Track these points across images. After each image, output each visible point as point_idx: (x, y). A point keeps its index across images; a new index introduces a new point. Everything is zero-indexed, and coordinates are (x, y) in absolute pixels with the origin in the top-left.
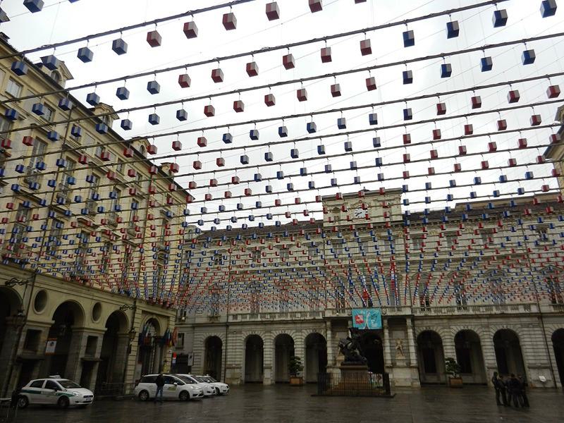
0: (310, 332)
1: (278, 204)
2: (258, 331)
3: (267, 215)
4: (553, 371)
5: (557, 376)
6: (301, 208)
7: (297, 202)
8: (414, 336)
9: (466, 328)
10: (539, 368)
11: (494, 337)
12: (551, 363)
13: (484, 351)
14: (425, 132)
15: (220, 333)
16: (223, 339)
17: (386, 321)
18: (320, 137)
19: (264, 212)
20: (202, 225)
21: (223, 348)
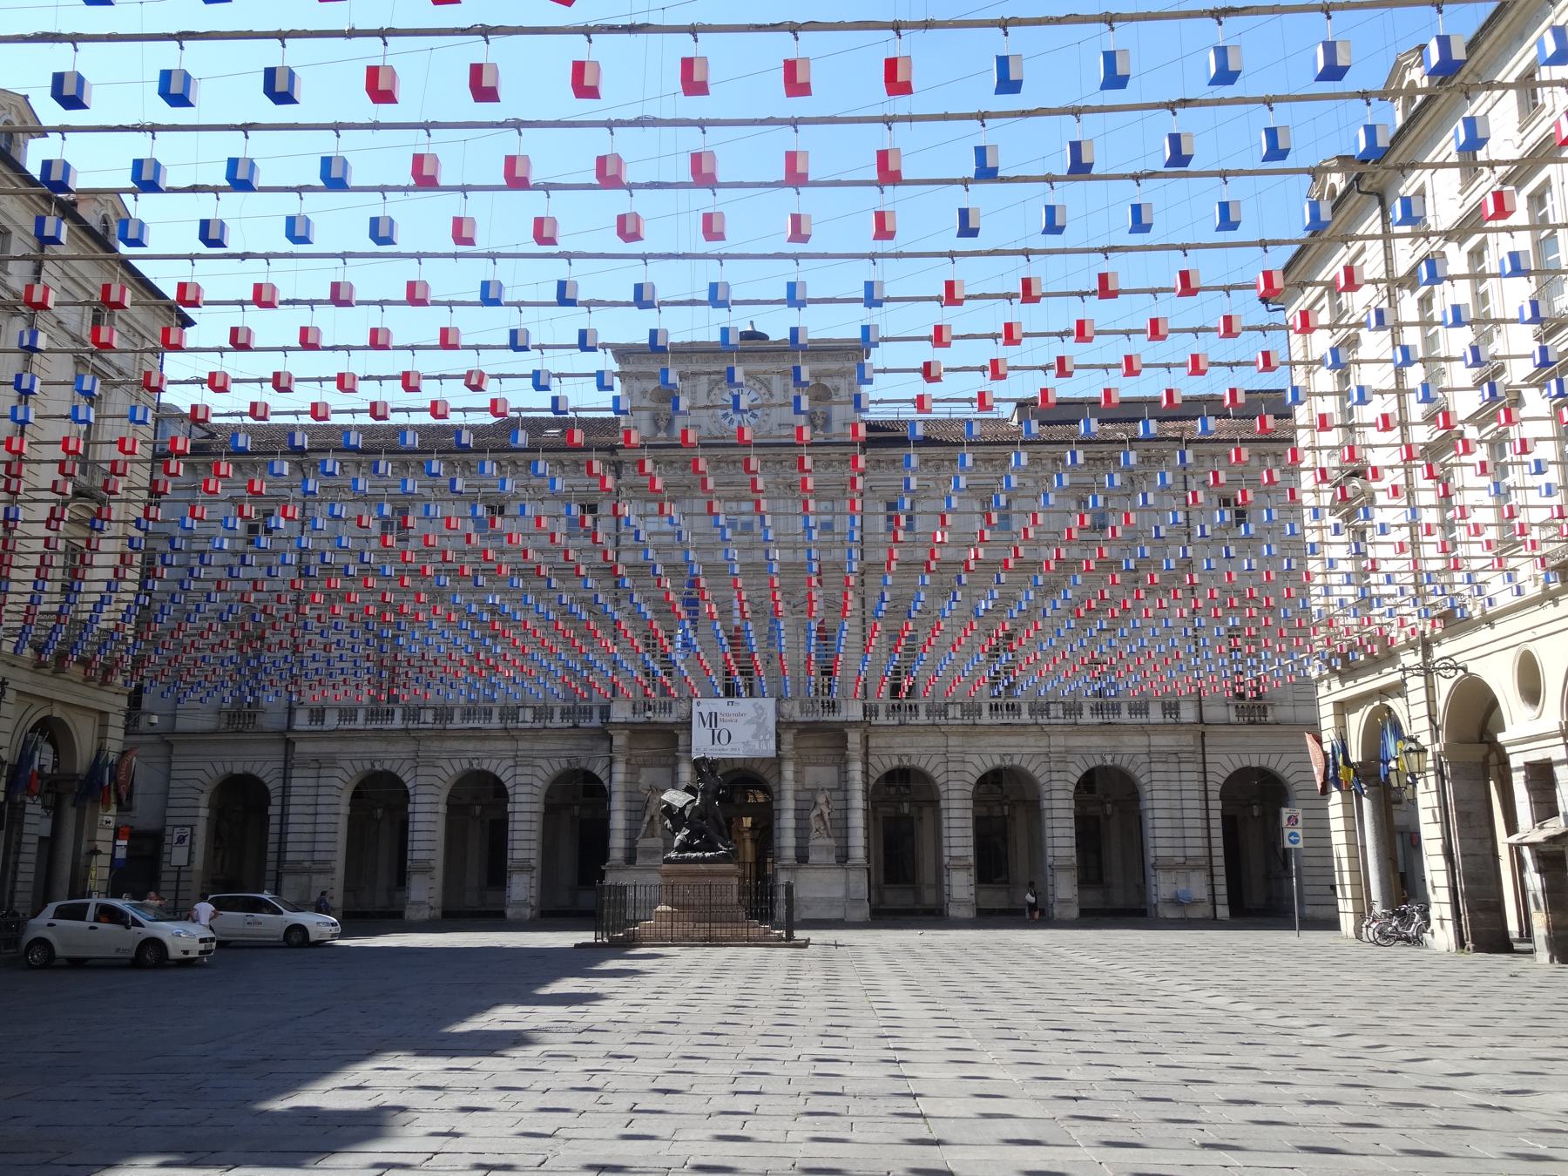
0: (559, 765)
1: (447, 341)
2: (393, 758)
3: (405, 377)
4: (1212, 876)
5: (1222, 890)
6: (458, 361)
7: (517, 342)
8: (866, 784)
9: (1008, 763)
10: (1186, 866)
11: (1077, 787)
12: (1210, 856)
13: (1048, 823)
14: (848, 152)
15: (263, 764)
16: (274, 785)
17: (788, 737)
18: (518, 125)
19: (265, 365)
20: (223, 389)
21: (274, 810)
